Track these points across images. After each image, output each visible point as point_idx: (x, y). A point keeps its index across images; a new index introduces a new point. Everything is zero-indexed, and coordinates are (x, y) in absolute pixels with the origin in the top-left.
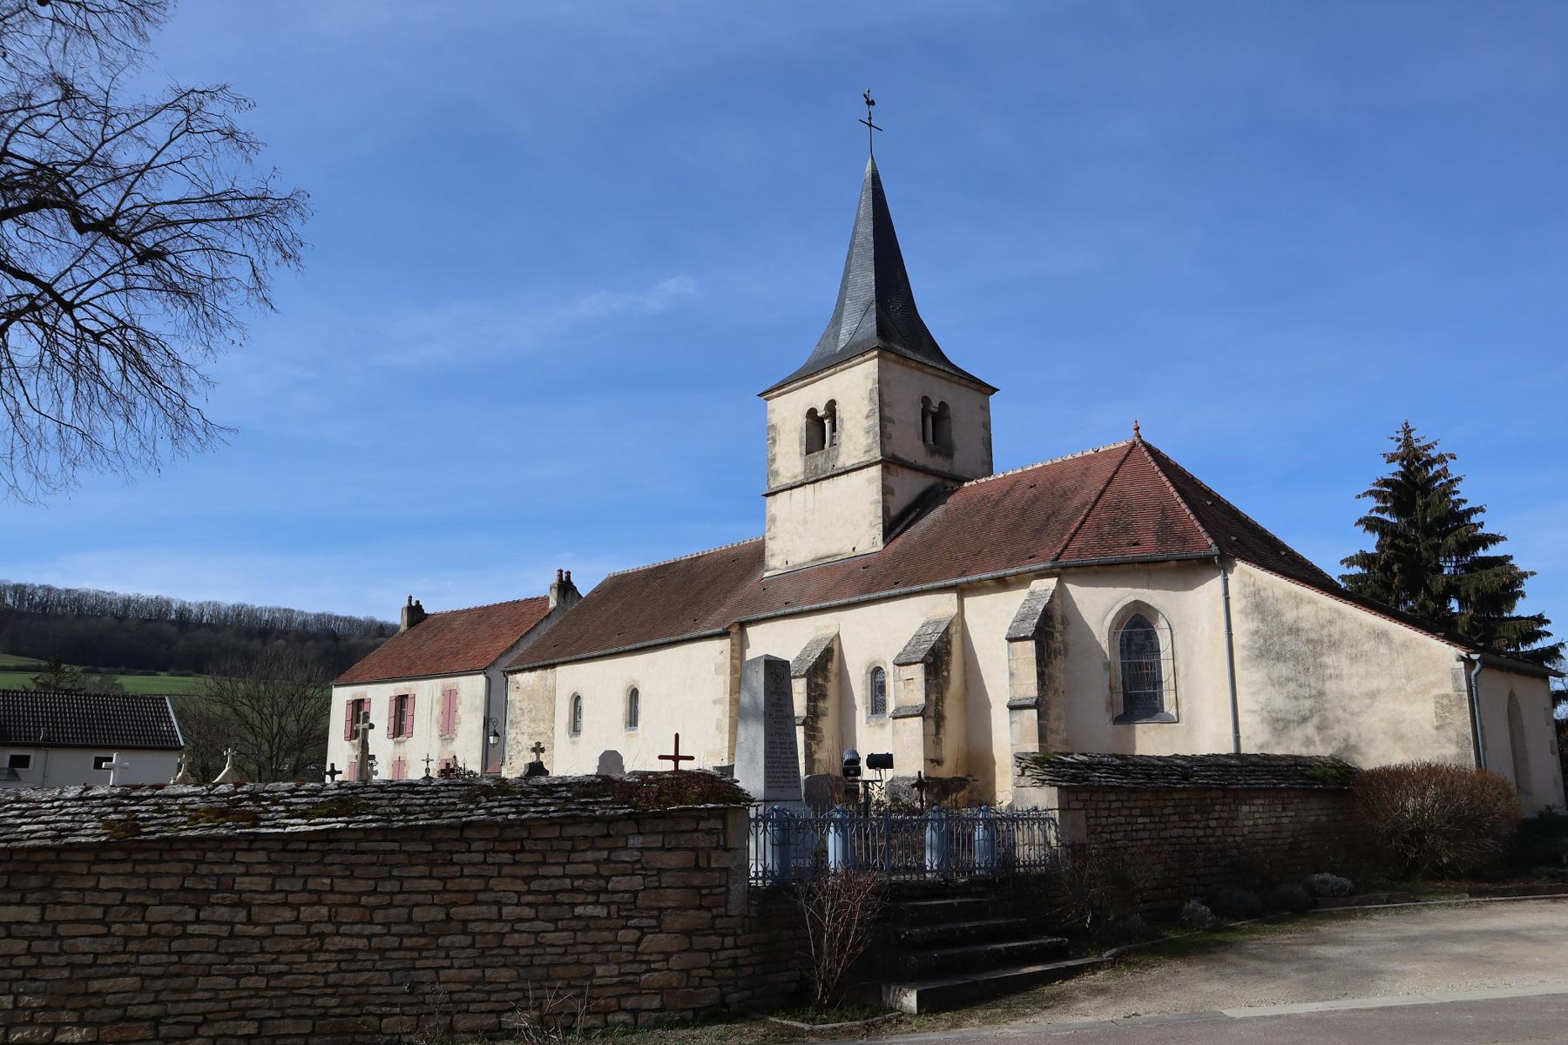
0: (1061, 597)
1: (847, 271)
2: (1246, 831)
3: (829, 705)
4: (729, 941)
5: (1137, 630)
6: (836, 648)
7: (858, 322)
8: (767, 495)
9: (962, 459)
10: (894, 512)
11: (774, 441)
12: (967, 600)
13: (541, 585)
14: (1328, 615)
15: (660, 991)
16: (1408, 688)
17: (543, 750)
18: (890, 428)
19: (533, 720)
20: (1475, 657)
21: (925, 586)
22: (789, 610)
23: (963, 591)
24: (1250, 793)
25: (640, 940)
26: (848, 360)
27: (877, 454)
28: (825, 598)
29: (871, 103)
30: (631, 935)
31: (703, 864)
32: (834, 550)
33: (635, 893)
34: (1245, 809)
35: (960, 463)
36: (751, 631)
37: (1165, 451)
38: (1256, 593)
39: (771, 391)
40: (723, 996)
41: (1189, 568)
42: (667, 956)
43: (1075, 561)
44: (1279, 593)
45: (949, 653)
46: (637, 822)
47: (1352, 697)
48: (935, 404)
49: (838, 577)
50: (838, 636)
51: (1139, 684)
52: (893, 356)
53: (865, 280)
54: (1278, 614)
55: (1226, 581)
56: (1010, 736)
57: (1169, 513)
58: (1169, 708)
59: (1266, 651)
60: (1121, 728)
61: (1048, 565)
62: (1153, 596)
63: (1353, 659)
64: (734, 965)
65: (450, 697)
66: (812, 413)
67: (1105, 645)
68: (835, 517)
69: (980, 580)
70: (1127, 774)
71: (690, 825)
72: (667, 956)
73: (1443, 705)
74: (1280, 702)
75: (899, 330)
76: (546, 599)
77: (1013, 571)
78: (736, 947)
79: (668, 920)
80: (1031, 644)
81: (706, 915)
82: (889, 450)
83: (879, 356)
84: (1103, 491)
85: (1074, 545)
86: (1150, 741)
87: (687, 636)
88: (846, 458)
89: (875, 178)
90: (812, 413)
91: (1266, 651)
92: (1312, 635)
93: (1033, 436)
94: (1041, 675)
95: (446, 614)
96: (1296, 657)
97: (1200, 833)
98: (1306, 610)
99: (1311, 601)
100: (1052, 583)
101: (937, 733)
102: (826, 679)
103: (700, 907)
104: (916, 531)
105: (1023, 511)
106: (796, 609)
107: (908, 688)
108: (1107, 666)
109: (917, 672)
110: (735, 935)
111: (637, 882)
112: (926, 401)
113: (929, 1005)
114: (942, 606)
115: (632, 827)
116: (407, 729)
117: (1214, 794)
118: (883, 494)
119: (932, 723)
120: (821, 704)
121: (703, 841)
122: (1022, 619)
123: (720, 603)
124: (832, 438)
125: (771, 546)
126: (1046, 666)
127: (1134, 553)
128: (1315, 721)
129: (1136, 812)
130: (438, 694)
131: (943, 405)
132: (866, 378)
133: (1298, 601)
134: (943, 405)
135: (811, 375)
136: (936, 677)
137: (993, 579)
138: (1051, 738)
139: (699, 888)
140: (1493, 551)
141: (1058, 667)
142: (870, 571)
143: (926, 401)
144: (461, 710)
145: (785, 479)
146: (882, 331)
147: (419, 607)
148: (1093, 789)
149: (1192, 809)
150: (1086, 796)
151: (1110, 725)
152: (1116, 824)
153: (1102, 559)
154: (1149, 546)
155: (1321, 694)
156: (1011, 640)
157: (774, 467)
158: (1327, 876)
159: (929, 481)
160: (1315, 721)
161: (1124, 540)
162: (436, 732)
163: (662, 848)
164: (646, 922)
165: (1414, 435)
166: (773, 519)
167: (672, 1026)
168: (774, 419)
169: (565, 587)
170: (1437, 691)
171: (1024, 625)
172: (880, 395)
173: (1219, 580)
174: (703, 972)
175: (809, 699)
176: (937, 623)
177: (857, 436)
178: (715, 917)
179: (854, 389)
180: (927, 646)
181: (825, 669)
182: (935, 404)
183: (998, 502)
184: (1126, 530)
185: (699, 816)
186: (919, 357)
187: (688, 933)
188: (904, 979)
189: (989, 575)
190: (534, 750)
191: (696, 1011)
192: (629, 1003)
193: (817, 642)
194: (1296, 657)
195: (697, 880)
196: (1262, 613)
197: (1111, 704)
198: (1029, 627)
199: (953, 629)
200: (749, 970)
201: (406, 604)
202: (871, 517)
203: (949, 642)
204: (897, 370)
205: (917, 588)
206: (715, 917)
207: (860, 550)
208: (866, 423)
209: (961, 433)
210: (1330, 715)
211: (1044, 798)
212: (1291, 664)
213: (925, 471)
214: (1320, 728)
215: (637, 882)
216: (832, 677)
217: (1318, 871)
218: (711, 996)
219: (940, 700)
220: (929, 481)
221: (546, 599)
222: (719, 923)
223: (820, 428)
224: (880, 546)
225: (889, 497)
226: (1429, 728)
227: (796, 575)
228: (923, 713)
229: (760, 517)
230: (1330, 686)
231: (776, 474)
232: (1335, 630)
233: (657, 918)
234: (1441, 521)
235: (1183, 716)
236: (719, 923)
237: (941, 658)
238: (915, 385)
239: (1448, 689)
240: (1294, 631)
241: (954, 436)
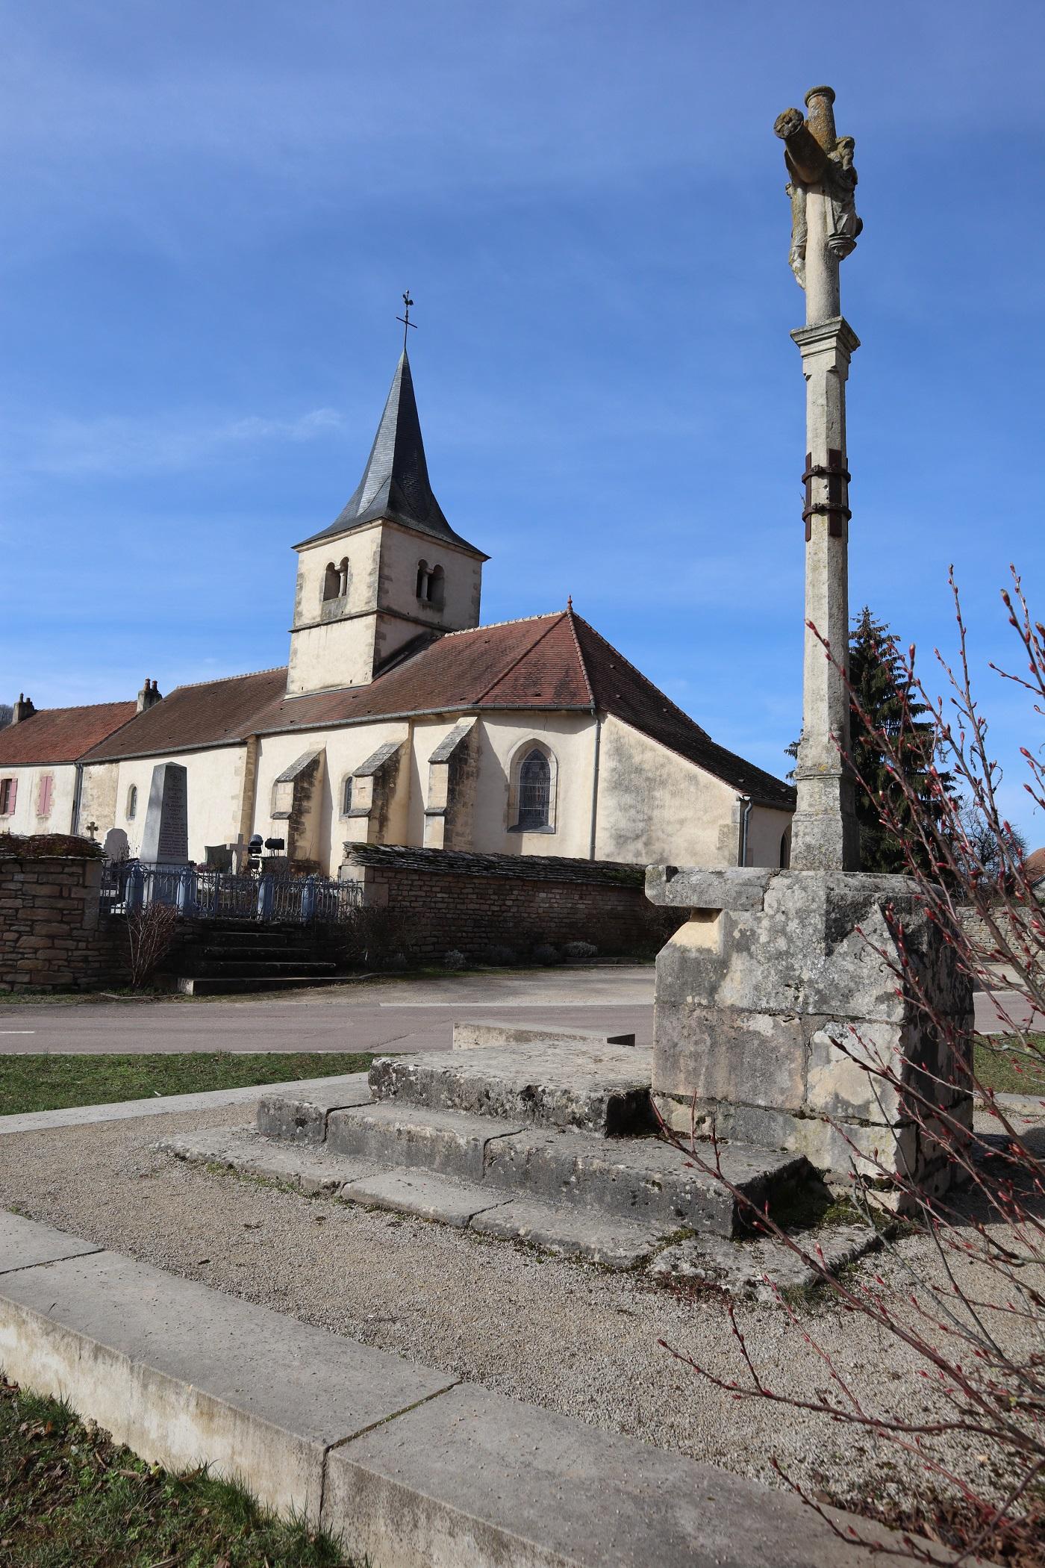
0: (479, 733)
2: (541, 911)
3: (313, 804)
4: (82, 945)
5: (535, 763)
6: (322, 760)
7: (374, 492)
8: (293, 632)
10: (384, 654)
12: (416, 729)
13: (131, 692)
14: (661, 760)
15: (30, 972)
16: (705, 819)
17: (96, 829)
18: (387, 585)
19: (100, 805)
20: (747, 798)
22: (291, 728)
23: (414, 722)
24: (547, 885)
25: (18, 939)
26: (360, 526)
27: (374, 606)
28: (319, 720)
30: (12, 936)
31: (65, 894)
32: (337, 682)
33: (17, 910)
34: (543, 895)
35: (448, 617)
36: (265, 743)
37: (591, 622)
38: (618, 740)
39: (302, 545)
40: (75, 979)
41: (574, 717)
42: (36, 951)
43: (491, 705)
44: (633, 742)
45: (397, 770)
46: (21, 865)
47: (669, 823)
48: (431, 567)
50: (324, 750)
51: (532, 806)
54: (630, 757)
55: (599, 729)
56: (346, 832)
57: (571, 673)
58: (551, 823)
59: (619, 785)
60: (513, 835)
62: (547, 737)
63: (673, 794)
64: (85, 960)
65: (46, 783)
66: (331, 566)
67: (507, 772)
68: (336, 655)
70: (431, 862)
71: (59, 869)
72: (36, 951)
73: (723, 835)
74: (623, 824)
76: (135, 703)
77: (451, 708)
78: (87, 949)
79: (38, 928)
80: (446, 767)
81: (66, 927)
82: (385, 603)
83: (383, 525)
84: (530, 651)
85: (496, 691)
86: (533, 845)
87: (221, 742)
89: (406, 371)
90: (331, 566)
91: (619, 785)
92: (650, 775)
93: (515, 594)
94: (451, 792)
95: (53, 711)
96: (637, 790)
97: (496, 908)
98: (648, 755)
99: (653, 749)
100: (472, 720)
101: (381, 830)
102: (311, 784)
103: (61, 922)
104: (398, 671)
105: (473, 661)
106: (296, 727)
107: (364, 795)
108: (508, 788)
109: (368, 783)
110: (88, 942)
111: (18, 903)
112: (423, 564)
113: (201, 991)
114: (394, 733)
115: (17, 868)
116: (10, 808)
117: (513, 883)
119: (376, 824)
120: (305, 804)
121: (66, 880)
122: (443, 747)
123: (248, 718)
125: (293, 674)
126: (458, 784)
127: (536, 702)
128: (644, 839)
129: (438, 889)
130: (37, 780)
131: (438, 568)
133: (644, 748)
134: (438, 568)
135: (332, 535)
138: (456, 840)
139: (61, 910)
140: (920, 719)
141: (468, 787)
143: (423, 564)
144: (55, 794)
145: (306, 620)
146: (393, 503)
147: (29, 704)
148: (399, 871)
149: (491, 891)
150: (391, 874)
151: (505, 833)
152: (416, 896)
153: (510, 705)
154: (547, 699)
155: (650, 818)
156: (432, 762)
158: (581, 944)
159: (420, 630)
160: (644, 839)
161: (532, 690)
162: (34, 813)
163: (37, 883)
164: (22, 928)
165: (872, 618)
166: (295, 652)
167: (34, 993)
168: (303, 568)
169: (151, 694)
170: (721, 822)
173: (593, 729)
174: (61, 963)
175: (295, 798)
176: (392, 745)
177: (361, 591)
178: (72, 929)
179: (362, 549)
180: (379, 763)
181: (311, 776)
182: (431, 567)
184: (535, 684)
185: (64, 864)
186: (421, 527)
187: (52, 937)
188: (190, 975)
190: (89, 828)
191: (54, 986)
192: (9, 978)
193: (308, 754)
194: (637, 790)
195: (60, 904)
196: (620, 755)
197: (507, 817)
198: (446, 754)
199: (402, 752)
200: (97, 965)
201: (18, 700)
202: (365, 657)
203: (398, 761)
204: (399, 537)
206: (72, 929)
207: (355, 683)
209: (451, 591)
210: (654, 835)
211: (356, 873)
212: (634, 795)
213: (416, 621)
214: (646, 844)
215: (18, 903)
216: (316, 783)
217: (576, 939)
218: (66, 978)
219: (386, 805)
220: (420, 630)
221: (135, 703)
222: (75, 933)
223: (336, 579)
224: (370, 681)
226: (713, 848)
227: (308, 699)
228: (369, 815)
229: (287, 652)
230: (656, 813)
231: (300, 614)
232: (665, 772)
233: (31, 926)
234: (881, 691)
235: (559, 829)
236: (75, 933)
237: (386, 773)
238: (413, 550)
239: (728, 821)
240: (639, 770)
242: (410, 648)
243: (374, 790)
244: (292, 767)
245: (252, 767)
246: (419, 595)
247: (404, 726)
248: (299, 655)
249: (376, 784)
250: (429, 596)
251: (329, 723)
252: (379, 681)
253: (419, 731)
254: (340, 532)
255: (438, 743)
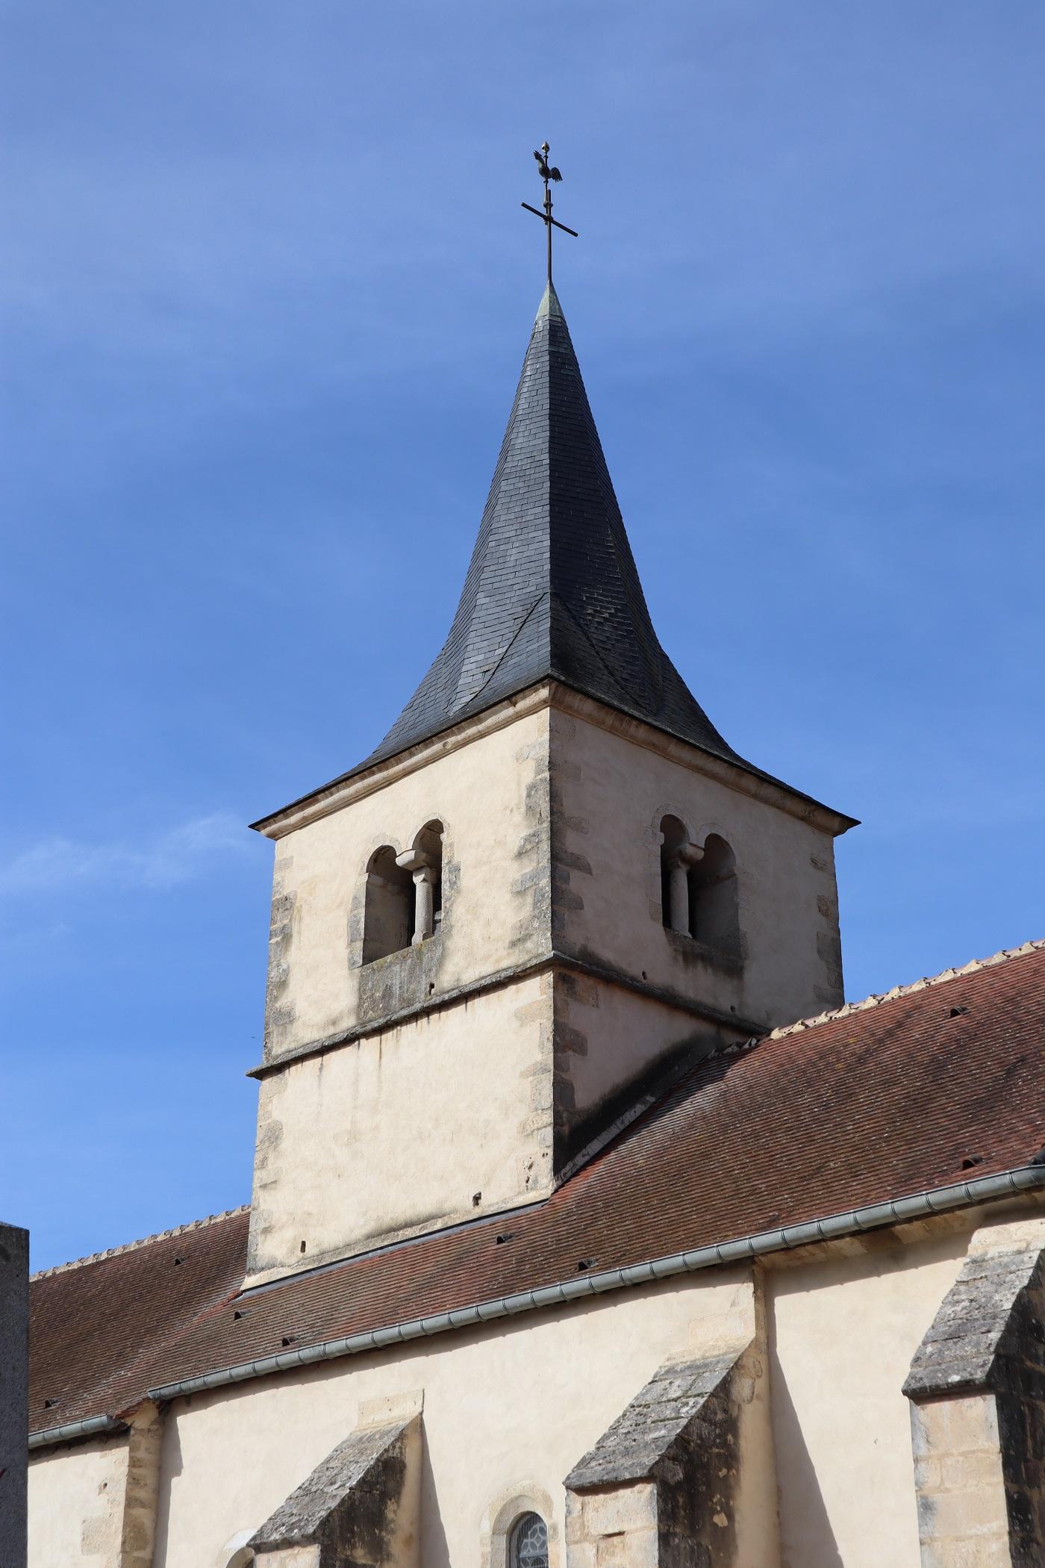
1: (486, 532)
6: (411, 1459)
8: (261, 1075)
9: (757, 989)
10: (586, 1098)
11: (287, 937)
12: (784, 1304)
18: (577, 883)
21: (663, 1265)
22: (289, 1357)
23: (772, 1273)
27: (542, 946)
29: (550, 174)
36: (189, 1425)
45: (731, 1458)
49: (430, 1268)
50: (418, 1425)
52: (589, 706)
53: (529, 551)
61: (1022, 1175)
66: (382, 859)
69: (820, 1240)
75: (601, 650)
77: (916, 1202)
80: (984, 1409)
82: (576, 938)
83: (553, 702)
88: (461, 966)
90: (382, 859)
104: (639, 1149)
105: (936, 1067)
106: (307, 1353)
109: (636, 1512)
112: (672, 827)
114: (712, 1320)
118: (558, 1048)
122: (951, 1333)
123: (122, 1359)
124: (433, 925)
126: (1033, 1481)
131: (715, 843)
132: (519, 758)
134: (715, 843)
136: (693, 1530)
137: (858, 1232)
142: (515, 1247)
143: (672, 827)
145: (307, 1032)
156: (920, 1395)
157: (283, 1003)
159: (682, 1028)
166: (274, 1136)
168: (288, 881)
171: (954, 1350)
172: (554, 796)
176: (697, 1369)
177: (493, 909)
179: (488, 793)
180: (666, 1433)
181: (376, 1520)
183: (861, 1060)
189: (844, 1220)
193: (360, 1443)
198: (977, 1356)
199: (743, 1388)
202: (523, 1112)
203: (731, 1425)
204: (603, 748)
205: (639, 1270)
207: (492, 1202)
208: (517, 871)
213: (669, 1001)
220: (682, 1028)
223: (402, 894)
224: (545, 1186)
225: (573, 1058)
227: (327, 1279)
229: (244, 1144)
231: (286, 1018)
238: (638, 786)
241: (744, 925)
242: (662, 1082)
243: (664, 1538)
244: (307, 1493)
245: (144, 1515)
246: (667, 921)
247: (740, 1294)
248: (286, 1144)
249: (667, 1515)
250: (693, 928)
251: (436, 1321)
252: (580, 1185)
253: (788, 1306)
254: (409, 749)
255: (923, 1327)
